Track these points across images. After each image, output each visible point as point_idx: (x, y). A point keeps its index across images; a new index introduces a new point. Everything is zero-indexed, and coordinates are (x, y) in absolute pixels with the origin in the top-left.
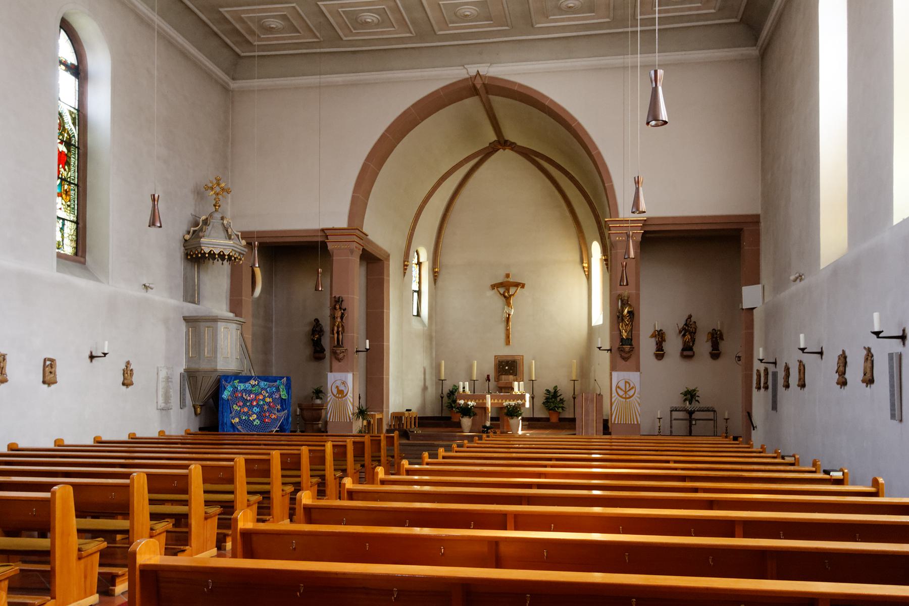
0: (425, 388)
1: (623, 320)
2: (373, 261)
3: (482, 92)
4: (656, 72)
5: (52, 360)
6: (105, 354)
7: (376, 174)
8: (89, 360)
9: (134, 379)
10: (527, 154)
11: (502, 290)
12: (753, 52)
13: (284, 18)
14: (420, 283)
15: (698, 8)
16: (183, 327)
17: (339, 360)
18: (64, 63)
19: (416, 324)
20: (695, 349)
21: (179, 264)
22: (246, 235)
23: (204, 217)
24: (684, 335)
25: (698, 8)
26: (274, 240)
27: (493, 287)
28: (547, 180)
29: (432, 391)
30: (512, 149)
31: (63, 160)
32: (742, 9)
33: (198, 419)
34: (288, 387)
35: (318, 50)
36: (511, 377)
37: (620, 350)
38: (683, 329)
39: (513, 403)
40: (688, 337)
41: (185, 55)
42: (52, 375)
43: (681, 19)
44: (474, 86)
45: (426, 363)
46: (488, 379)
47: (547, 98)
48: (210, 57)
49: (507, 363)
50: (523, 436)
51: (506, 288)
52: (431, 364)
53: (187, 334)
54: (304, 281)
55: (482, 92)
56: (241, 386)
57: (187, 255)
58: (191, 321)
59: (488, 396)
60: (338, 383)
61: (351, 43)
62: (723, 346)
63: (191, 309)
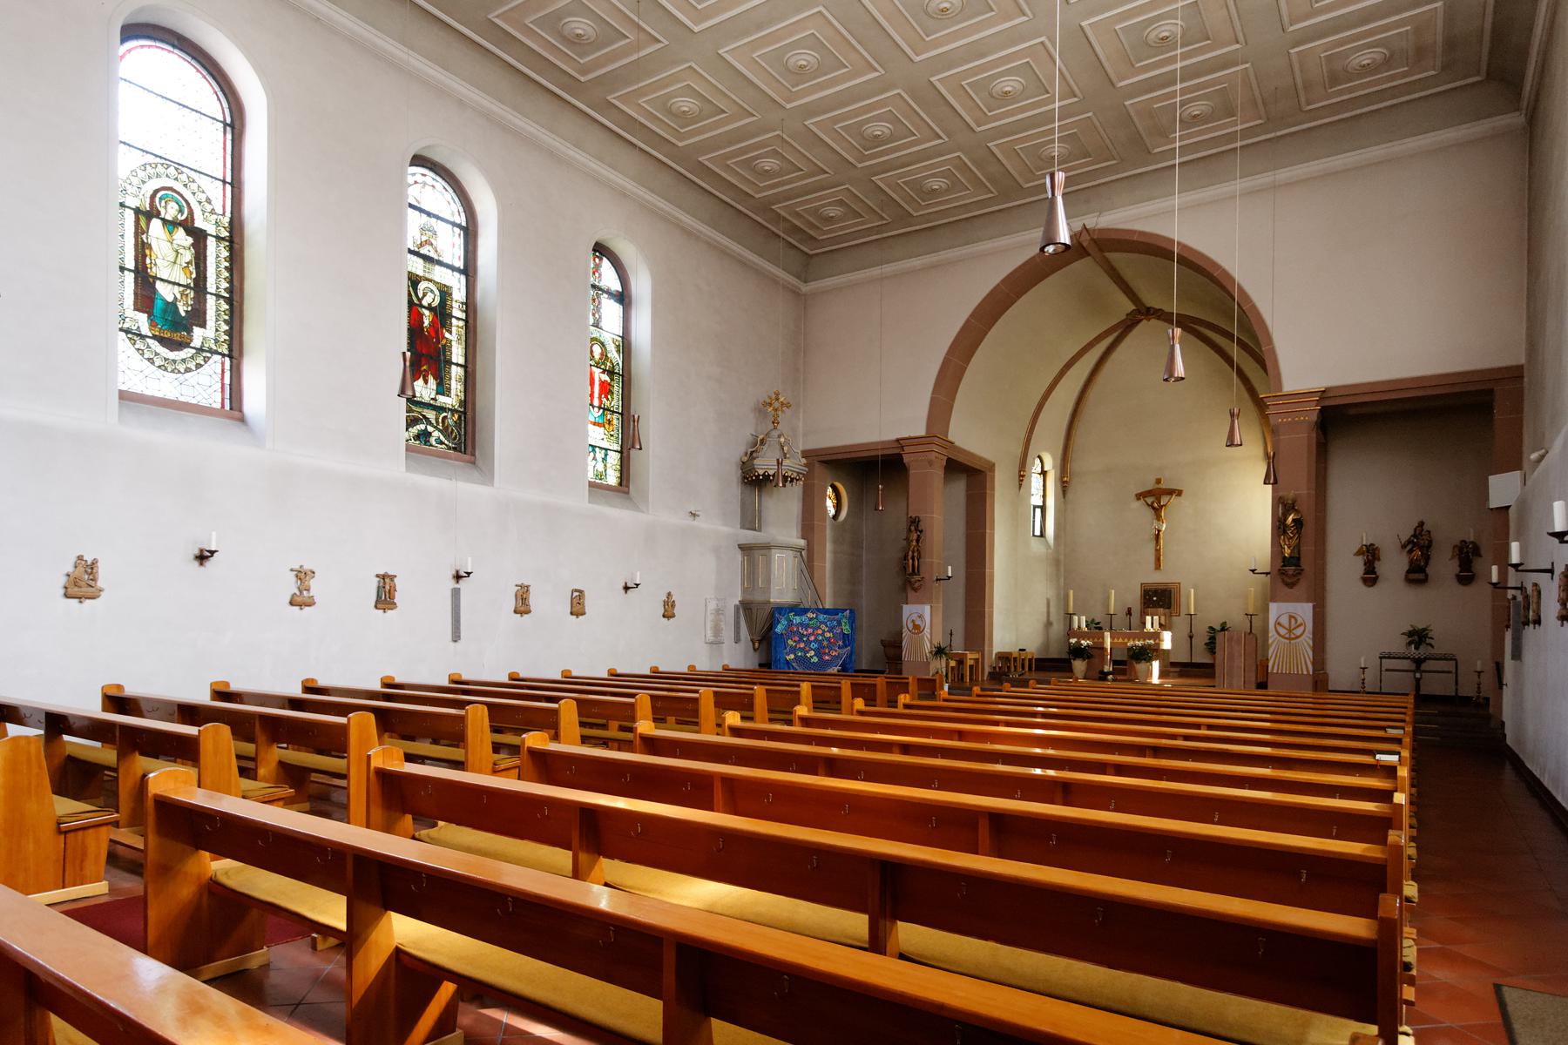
0: (1049, 624)
1: (1285, 532)
2: (971, 475)
3: (1092, 249)
4: (1052, 176)
5: (581, 592)
7: (963, 370)
11: (1150, 500)
12: (1516, 119)
13: (841, 203)
14: (1044, 496)
15: (1404, 75)
16: (739, 556)
17: (915, 590)
18: (608, 292)
19: (1036, 546)
20: (1428, 570)
21: (735, 489)
22: (806, 454)
24: (1410, 552)
25: (1404, 75)
27: (1139, 496)
30: (1158, 318)
31: (606, 389)
32: (1485, 58)
33: (757, 655)
34: (852, 621)
37: (1282, 573)
38: (1409, 542)
39: (1139, 643)
41: (743, 263)
43: (1381, 95)
45: (1051, 593)
46: (1129, 612)
48: (775, 262)
49: (1156, 592)
50: (1159, 688)
51: (1157, 497)
52: (1058, 595)
54: (891, 501)
55: (1092, 249)
56: (797, 620)
58: (746, 549)
59: (1107, 635)
60: (914, 617)
63: (749, 536)
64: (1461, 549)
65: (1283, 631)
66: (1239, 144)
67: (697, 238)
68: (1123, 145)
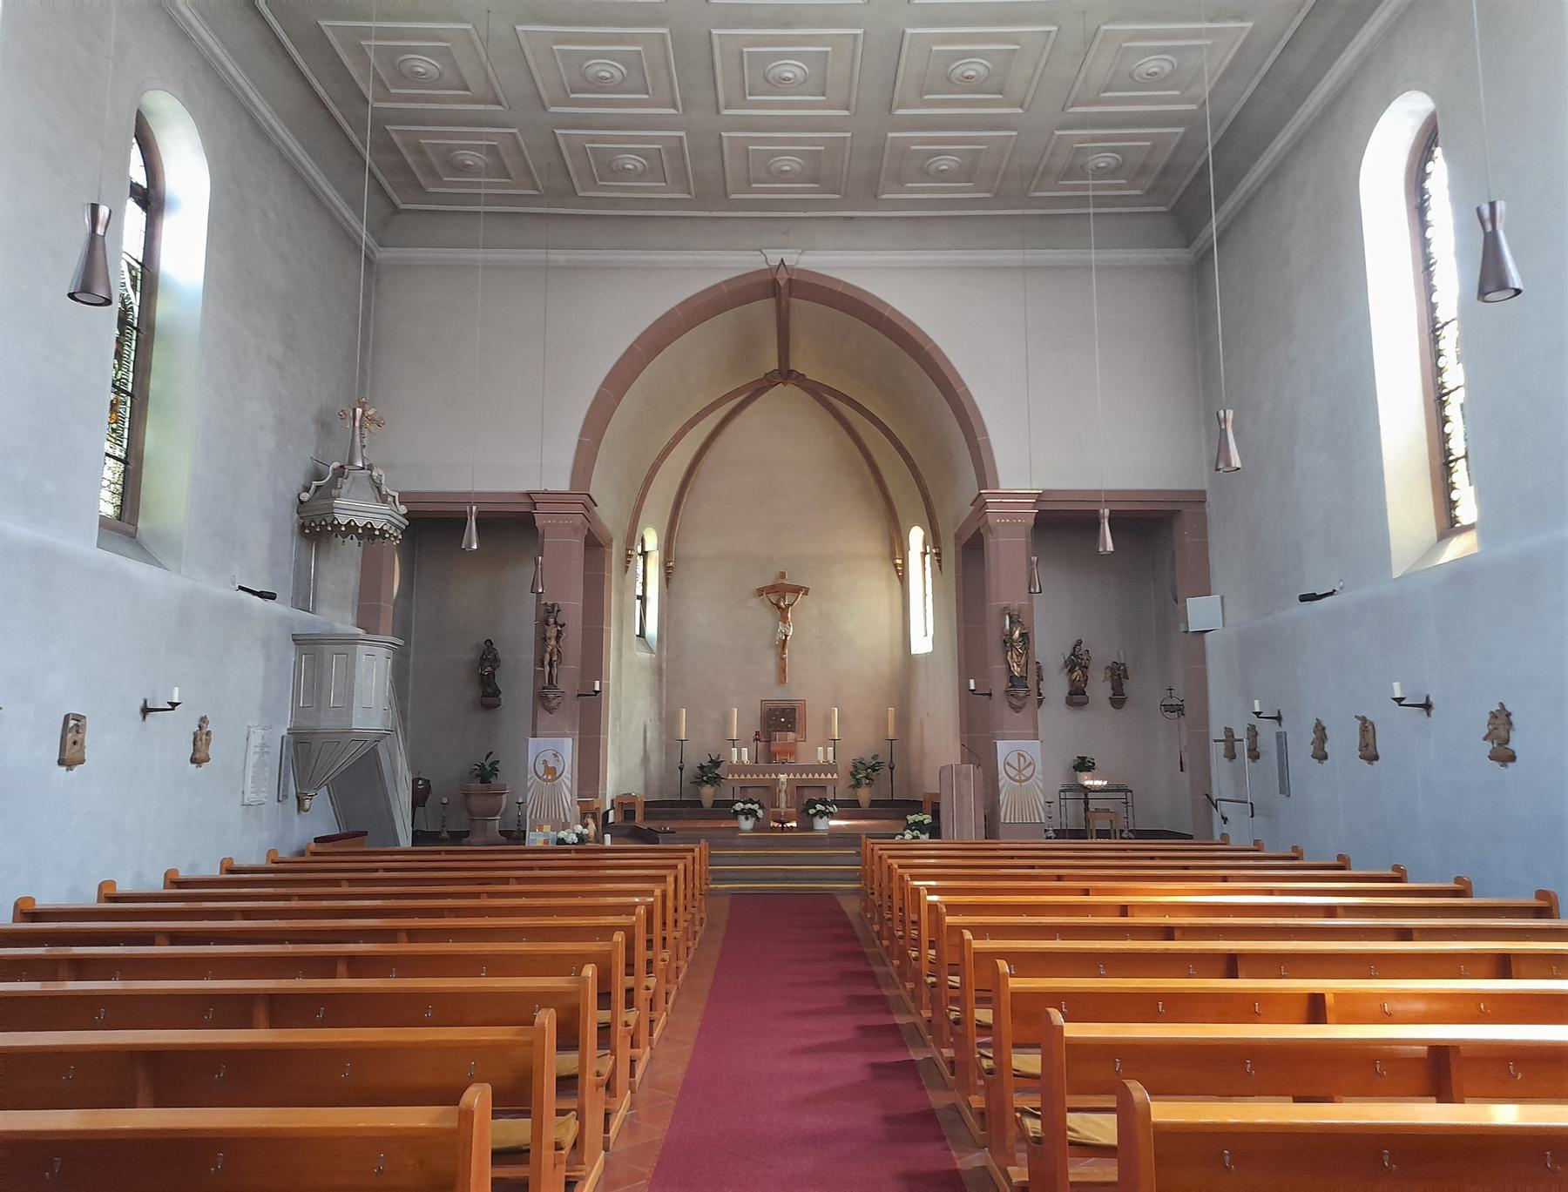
0: (646, 759)
6: (174, 705)
8: (140, 716)
9: (212, 751)
10: (816, 391)
13: (493, 151)
14: (644, 584)
15: (1120, 187)
17: (550, 710)
21: (289, 544)
23: (336, 464)
24: (1071, 671)
25: (1120, 187)
26: (432, 508)
28: (840, 428)
29: (655, 759)
35: (544, 210)
36: (791, 735)
40: (1077, 674)
42: (76, 747)
44: (775, 282)
47: (887, 305)
51: (780, 595)
53: (297, 664)
57: (303, 527)
60: (549, 755)
61: (590, 202)
62: (1128, 687)
64: (1112, 670)
65: (1013, 773)
66: (1092, 211)
67: (268, 140)
68: (859, 180)
